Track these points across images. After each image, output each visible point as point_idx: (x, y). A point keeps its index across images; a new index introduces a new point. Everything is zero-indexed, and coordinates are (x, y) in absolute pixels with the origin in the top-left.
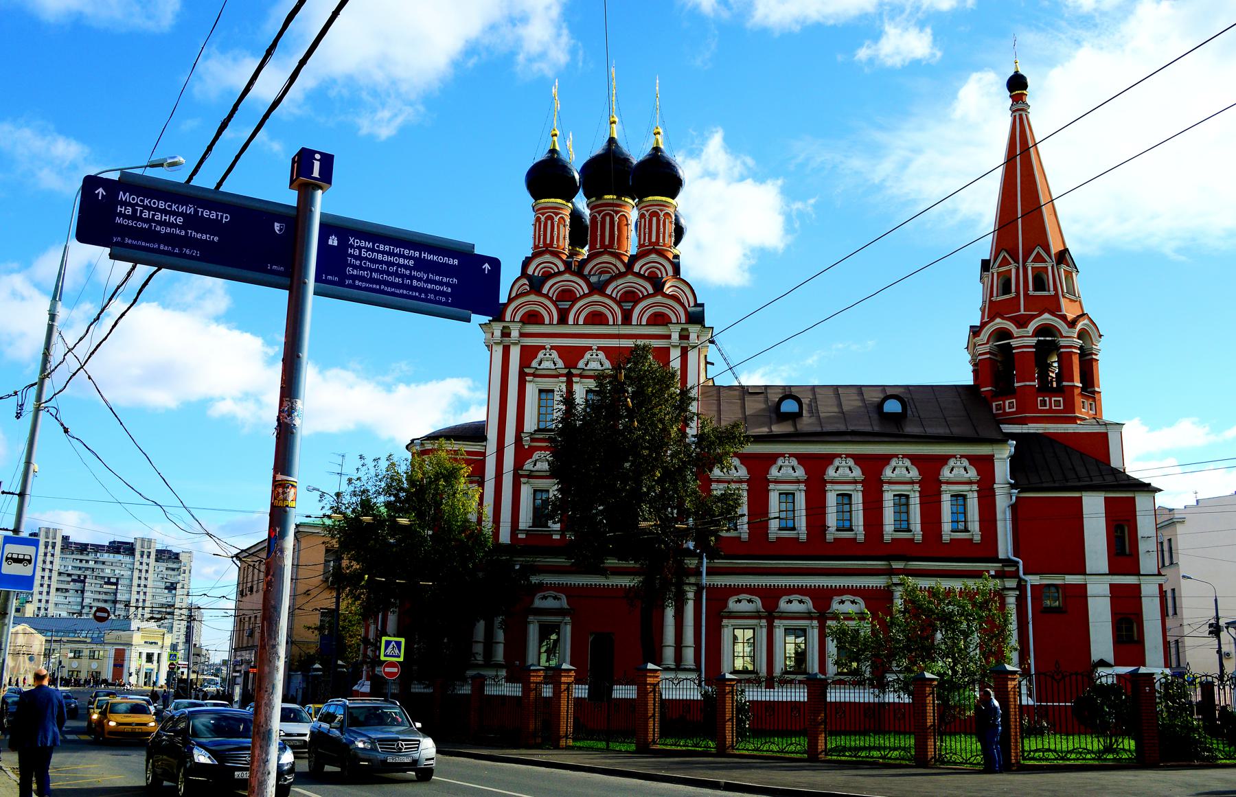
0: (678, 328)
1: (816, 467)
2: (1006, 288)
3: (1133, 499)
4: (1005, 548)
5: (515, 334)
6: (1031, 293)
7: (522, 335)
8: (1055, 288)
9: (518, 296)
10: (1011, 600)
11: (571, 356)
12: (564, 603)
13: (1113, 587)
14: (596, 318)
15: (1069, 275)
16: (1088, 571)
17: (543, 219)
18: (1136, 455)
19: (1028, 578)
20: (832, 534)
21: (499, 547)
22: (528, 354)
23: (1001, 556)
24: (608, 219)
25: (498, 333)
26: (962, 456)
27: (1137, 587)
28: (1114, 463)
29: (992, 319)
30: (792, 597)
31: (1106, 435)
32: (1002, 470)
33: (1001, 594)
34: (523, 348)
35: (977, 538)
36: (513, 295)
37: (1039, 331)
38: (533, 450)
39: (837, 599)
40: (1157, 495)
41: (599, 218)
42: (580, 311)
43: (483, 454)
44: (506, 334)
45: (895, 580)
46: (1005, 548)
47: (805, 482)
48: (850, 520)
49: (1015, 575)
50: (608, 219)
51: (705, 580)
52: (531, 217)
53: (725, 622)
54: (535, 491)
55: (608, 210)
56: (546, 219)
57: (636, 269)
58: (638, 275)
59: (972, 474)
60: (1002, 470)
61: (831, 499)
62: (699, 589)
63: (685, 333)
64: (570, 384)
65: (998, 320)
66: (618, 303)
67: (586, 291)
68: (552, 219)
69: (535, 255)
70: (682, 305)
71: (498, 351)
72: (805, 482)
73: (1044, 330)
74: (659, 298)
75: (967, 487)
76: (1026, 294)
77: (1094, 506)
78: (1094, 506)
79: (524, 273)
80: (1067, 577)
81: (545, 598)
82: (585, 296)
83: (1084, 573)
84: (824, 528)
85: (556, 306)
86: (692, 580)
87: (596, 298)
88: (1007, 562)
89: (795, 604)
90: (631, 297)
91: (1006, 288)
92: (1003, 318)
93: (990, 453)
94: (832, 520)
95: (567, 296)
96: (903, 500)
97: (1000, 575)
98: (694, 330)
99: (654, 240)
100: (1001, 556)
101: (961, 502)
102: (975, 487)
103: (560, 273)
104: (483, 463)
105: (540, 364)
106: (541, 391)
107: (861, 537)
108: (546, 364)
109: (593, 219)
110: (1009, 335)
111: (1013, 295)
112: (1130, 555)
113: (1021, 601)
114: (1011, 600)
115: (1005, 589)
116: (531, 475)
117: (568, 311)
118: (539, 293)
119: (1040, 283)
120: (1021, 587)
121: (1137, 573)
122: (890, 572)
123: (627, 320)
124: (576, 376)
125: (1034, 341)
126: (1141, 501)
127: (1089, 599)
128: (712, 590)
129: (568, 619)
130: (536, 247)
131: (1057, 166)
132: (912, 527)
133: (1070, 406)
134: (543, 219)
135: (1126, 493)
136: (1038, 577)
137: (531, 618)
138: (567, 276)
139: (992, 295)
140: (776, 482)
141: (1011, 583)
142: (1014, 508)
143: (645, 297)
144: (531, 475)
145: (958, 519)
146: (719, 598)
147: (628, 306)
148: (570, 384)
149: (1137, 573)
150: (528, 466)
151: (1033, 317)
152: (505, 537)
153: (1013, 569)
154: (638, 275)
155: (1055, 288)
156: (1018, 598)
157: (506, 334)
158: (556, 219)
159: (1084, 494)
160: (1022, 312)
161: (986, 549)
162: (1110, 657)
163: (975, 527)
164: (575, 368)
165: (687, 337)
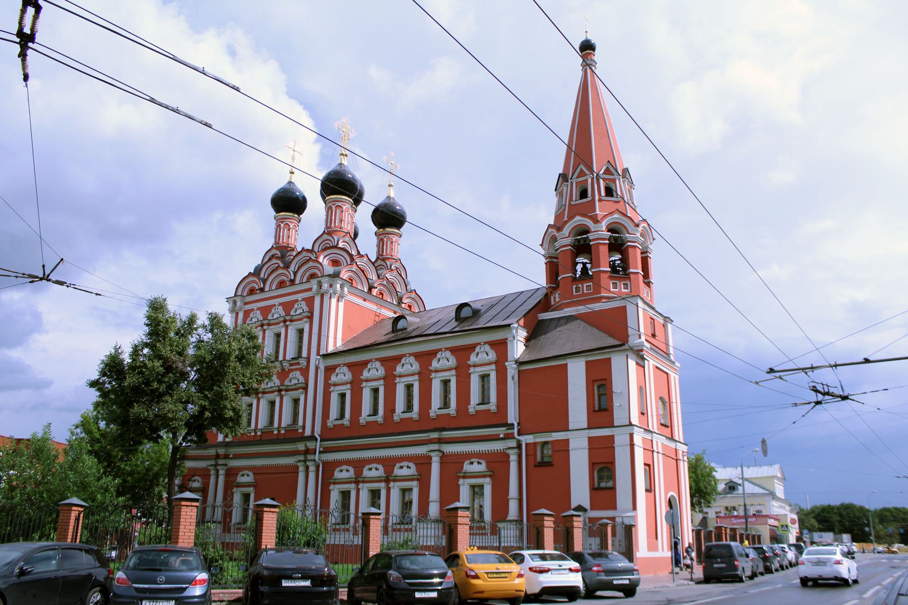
1: (424, 358)
4: (512, 416)
13: (591, 439)
16: (570, 428)
26: (485, 343)
27: (611, 438)
29: (571, 218)
46: (512, 416)
53: (461, 481)
65: (578, 218)
70: (347, 252)
71: (234, 315)
80: (554, 434)
89: (475, 464)
111: (589, 199)
114: (513, 458)
121: (566, 429)
127: (571, 452)
133: (598, 288)
136: (531, 436)
139: (571, 200)
141: (513, 443)
146: (329, 469)
149: (612, 426)
161: (498, 419)
162: (586, 504)
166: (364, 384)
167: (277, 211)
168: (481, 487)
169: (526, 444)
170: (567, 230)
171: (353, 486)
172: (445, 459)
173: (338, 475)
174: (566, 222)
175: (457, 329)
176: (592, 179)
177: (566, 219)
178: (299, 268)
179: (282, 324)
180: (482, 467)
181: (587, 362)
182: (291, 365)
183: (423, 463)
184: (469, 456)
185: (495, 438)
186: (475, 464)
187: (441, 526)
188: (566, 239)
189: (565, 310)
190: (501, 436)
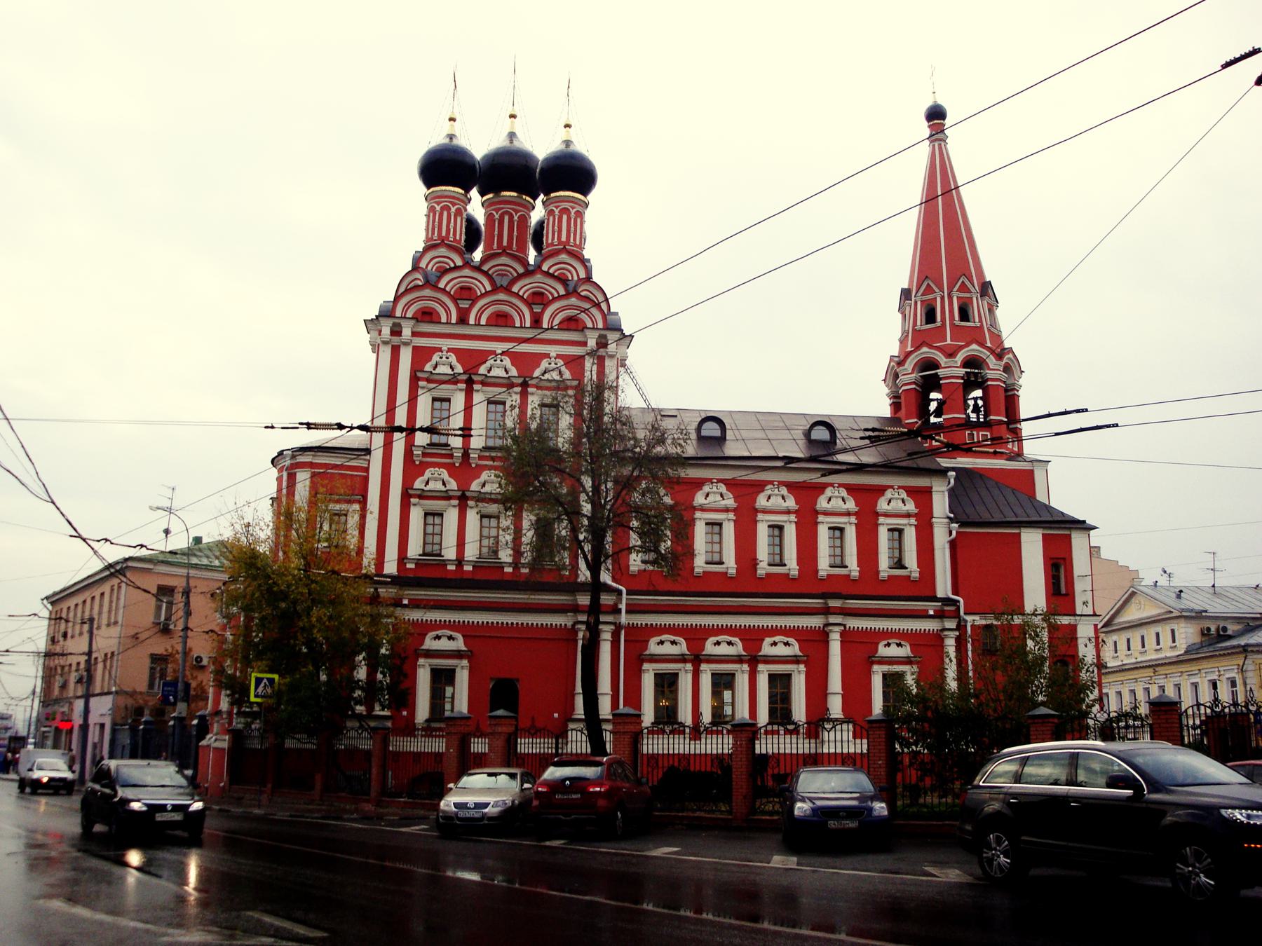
0: (596, 334)
1: (745, 492)
2: (930, 316)
3: (1069, 536)
4: (943, 586)
5: (406, 332)
6: (957, 322)
7: (414, 334)
8: (980, 321)
9: (407, 291)
10: (950, 645)
11: (526, 363)
12: (459, 644)
14: (501, 319)
15: (991, 311)
17: (438, 208)
18: (1062, 492)
19: (969, 618)
20: (763, 569)
21: (377, 578)
22: (421, 355)
23: (940, 594)
24: (506, 218)
25: (386, 331)
26: (899, 487)
28: (1041, 496)
29: (918, 348)
30: (719, 638)
31: (1032, 471)
32: (941, 504)
33: (938, 638)
34: (416, 350)
35: (915, 575)
36: (402, 290)
37: (967, 363)
38: (480, 469)
39: (768, 640)
40: (1092, 532)
41: (497, 216)
42: (480, 313)
43: (367, 470)
44: (396, 332)
45: (832, 619)
46: (943, 586)
47: (734, 510)
48: (720, 552)
49: (956, 615)
50: (506, 218)
51: (624, 619)
52: (423, 207)
54: (426, 514)
55: (507, 207)
56: (442, 209)
57: (545, 268)
58: (547, 274)
59: (911, 506)
60: (941, 504)
61: (763, 532)
62: (618, 628)
63: (397, 329)
64: (524, 395)
65: (925, 349)
66: (454, 300)
67: (489, 288)
68: (448, 209)
69: (427, 249)
71: (386, 353)
72: (734, 510)
73: (971, 362)
74: (573, 301)
75: (904, 521)
76: (952, 325)
77: (1032, 545)
78: (1032, 545)
79: (416, 268)
81: (438, 637)
82: (487, 293)
83: (1075, 615)
84: (754, 563)
85: (457, 305)
86: (610, 618)
87: (501, 296)
88: (947, 601)
89: (893, 647)
90: (466, 293)
91: (930, 316)
92: (930, 347)
93: (928, 485)
94: (763, 552)
95: (466, 293)
96: (837, 533)
97: (940, 615)
98: (612, 336)
99: (505, 243)
100: (940, 594)
101: (896, 534)
102: (913, 521)
103: (456, 268)
104: (366, 479)
105: (489, 371)
106: (434, 399)
107: (915, 575)
108: (440, 369)
109: (489, 218)
110: (934, 365)
111: (939, 324)
112: (1066, 595)
113: (961, 644)
114: (950, 645)
115: (944, 629)
116: (423, 496)
117: (468, 310)
118: (435, 287)
119: (964, 315)
120: (961, 627)
122: (826, 611)
123: (463, 320)
124: (478, 382)
125: (962, 371)
126: (1078, 540)
128: (631, 629)
129: (802, 667)
130: (428, 239)
131: (978, 205)
132: (847, 562)
134: (438, 208)
135: (1061, 530)
137: (421, 661)
138: (467, 272)
140: (765, 512)
141: (951, 624)
142: (953, 544)
143: (555, 300)
144: (423, 496)
145: (895, 552)
146: (638, 638)
147: (464, 304)
148: (524, 395)
150: (419, 484)
151: (961, 347)
152: (391, 568)
153: (953, 608)
154: (547, 274)
155: (980, 321)
156: (958, 639)
157: (396, 332)
158: (453, 209)
159: (1023, 530)
160: (949, 342)
161: (923, 588)
163: (911, 560)
164: (476, 374)
165: (605, 345)
166: (698, 514)
167: (428, 186)
168: (675, 676)
169: (972, 626)
170: (909, 365)
171: (761, 667)
172: (848, 637)
173: (653, 648)
174: (910, 353)
175: (904, 464)
176: (942, 298)
177: (909, 349)
178: (407, 291)
179: (463, 386)
180: (905, 651)
181: (1044, 535)
182: (481, 458)
183: (815, 643)
184: (887, 635)
185: (922, 615)
186: (893, 647)
187: (851, 726)
188: (909, 375)
189: (959, 459)
190: (931, 612)
